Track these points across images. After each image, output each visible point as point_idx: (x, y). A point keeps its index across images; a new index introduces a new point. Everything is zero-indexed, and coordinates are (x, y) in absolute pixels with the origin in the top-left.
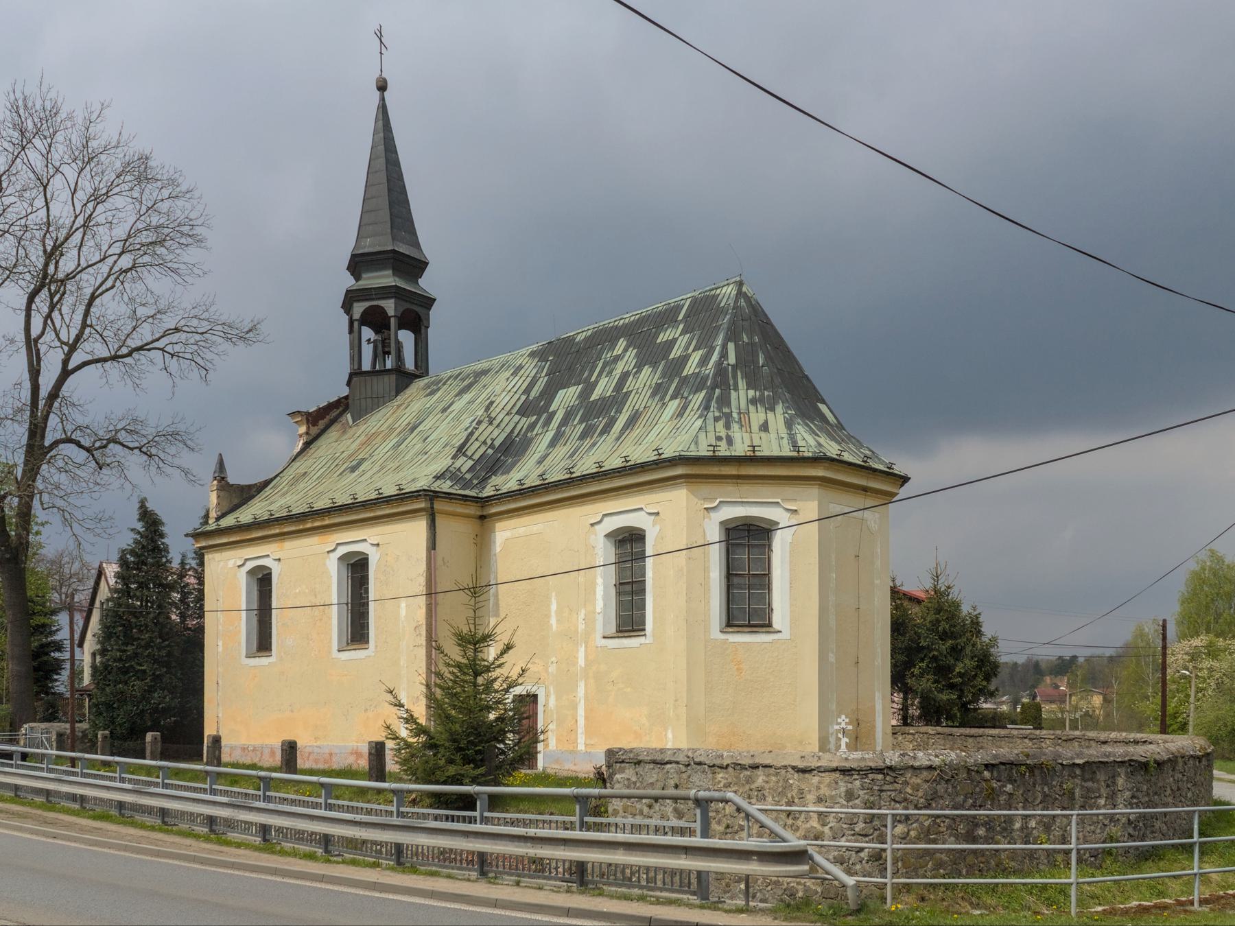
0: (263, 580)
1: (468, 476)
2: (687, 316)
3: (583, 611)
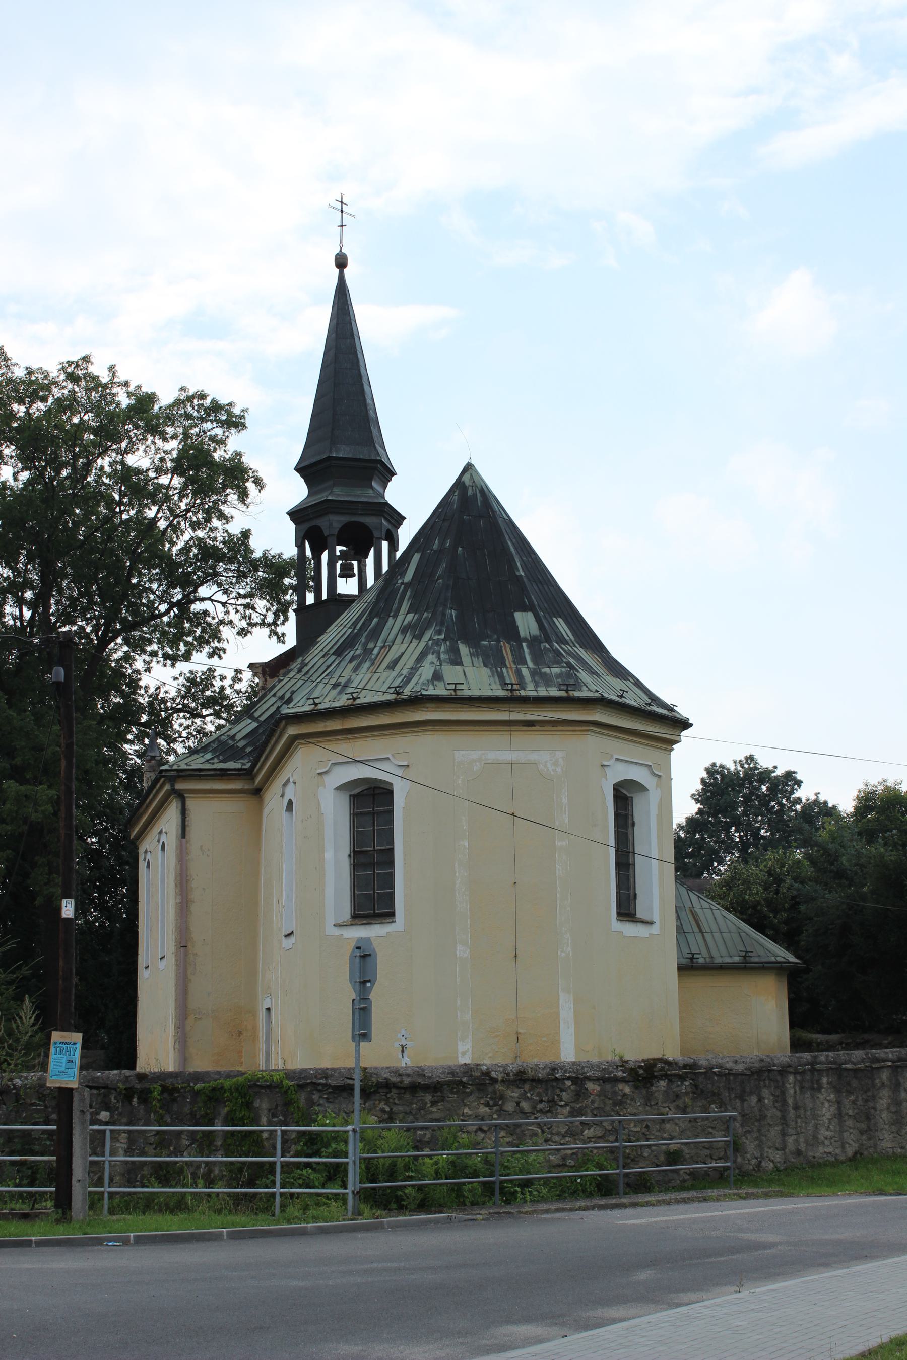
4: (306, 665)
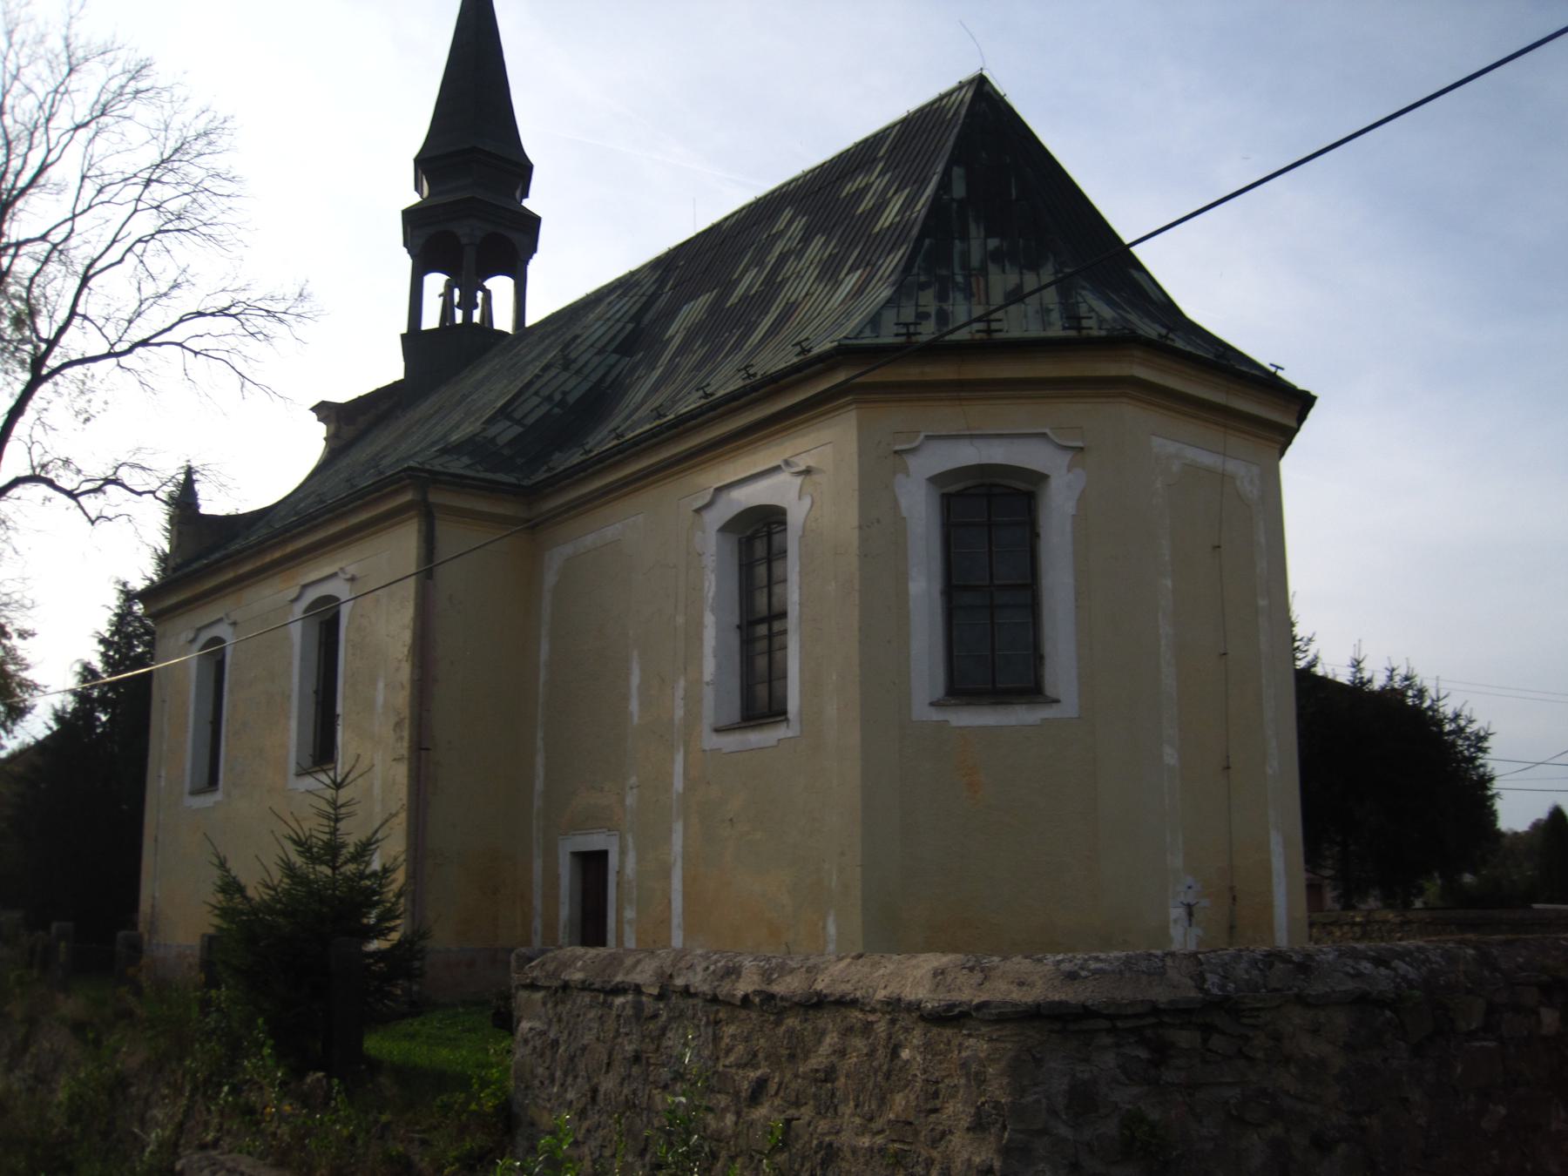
1: (506, 452)
2: (891, 151)
3: (682, 683)
4: (575, 361)
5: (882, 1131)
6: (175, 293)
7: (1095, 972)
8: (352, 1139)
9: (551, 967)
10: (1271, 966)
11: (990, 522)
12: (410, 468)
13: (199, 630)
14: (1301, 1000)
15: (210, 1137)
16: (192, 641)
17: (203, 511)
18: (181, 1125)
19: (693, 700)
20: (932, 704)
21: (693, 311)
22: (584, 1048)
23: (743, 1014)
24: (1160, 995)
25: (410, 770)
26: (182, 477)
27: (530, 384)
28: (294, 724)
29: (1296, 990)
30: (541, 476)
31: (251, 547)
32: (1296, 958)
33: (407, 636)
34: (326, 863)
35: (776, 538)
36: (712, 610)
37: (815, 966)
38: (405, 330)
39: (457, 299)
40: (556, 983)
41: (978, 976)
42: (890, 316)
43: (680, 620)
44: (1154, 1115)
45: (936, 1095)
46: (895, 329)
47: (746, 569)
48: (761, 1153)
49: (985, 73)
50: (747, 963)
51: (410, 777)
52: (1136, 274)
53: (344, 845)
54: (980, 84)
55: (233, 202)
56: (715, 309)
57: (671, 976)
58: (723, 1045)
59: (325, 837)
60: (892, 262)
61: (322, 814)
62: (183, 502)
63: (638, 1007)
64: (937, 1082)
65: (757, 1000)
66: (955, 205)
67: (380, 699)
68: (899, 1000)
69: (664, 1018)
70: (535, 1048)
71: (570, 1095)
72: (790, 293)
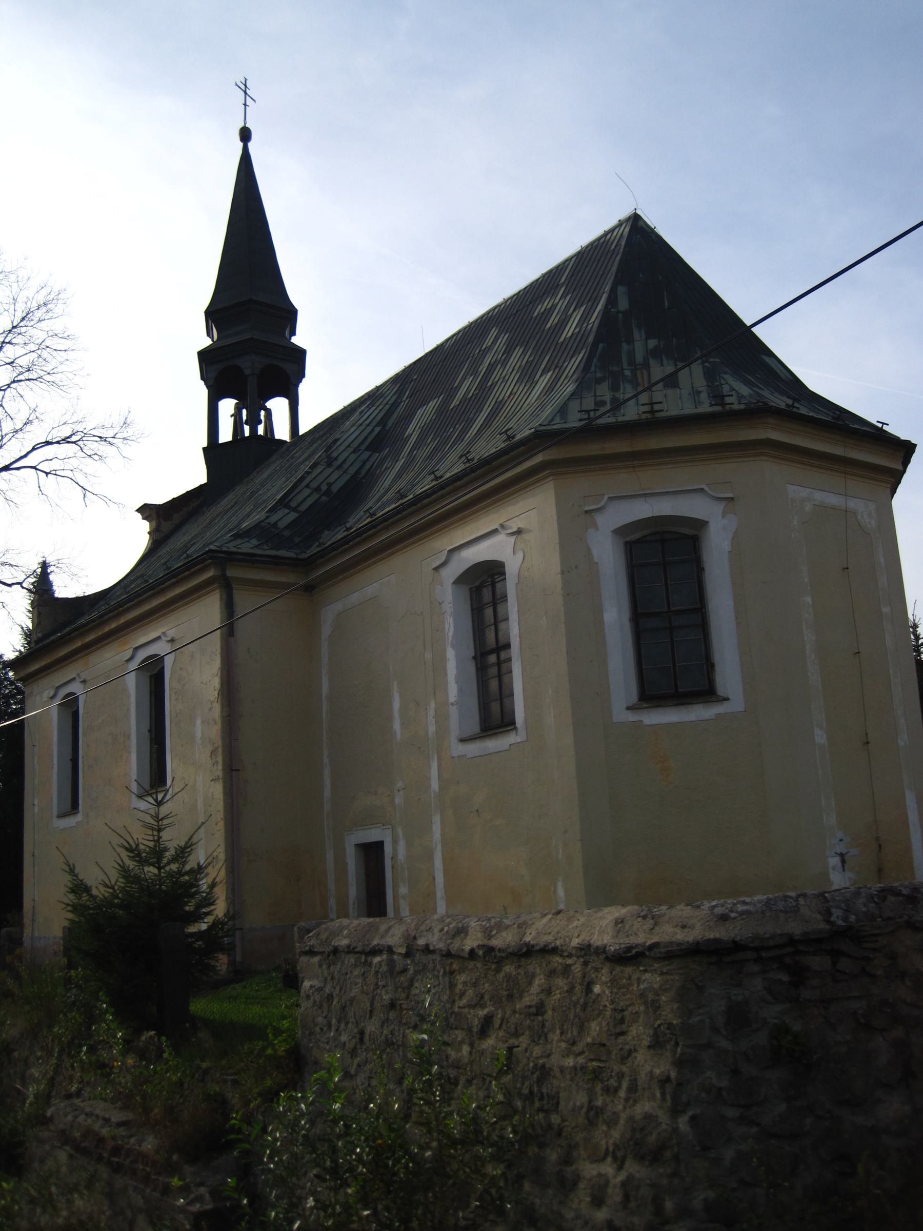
0: (71, 706)
1: (286, 533)
5: (582, 1053)
6: (29, 427)
7: (742, 913)
8: (181, 1084)
9: (323, 937)
10: (884, 899)
11: (664, 562)
12: (210, 551)
13: (58, 688)
14: (911, 925)
15: (74, 1088)
16: (52, 698)
17: (56, 595)
18: (52, 1080)
19: (441, 718)
20: (628, 708)
21: (426, 413)
22: (352, 1000)
23: (471, 964)
24: (795, 928)
25: (225, 787)
26: (39, 570)
27: (302, 479)
28: (134, 757)
29: (906, 918)
30: (314, 550)
31: (93, 621)
32: (905, 892)
33: (216, 682)
34: (153, 865)
35: (498, 586)
36: (453, 646)
37: (525, 923)
38: (205, 445)
39: (244, 418)
40: (327, 949)
41: (650, 923)
42: (574, 405)
43: (428, 656)
44: (797, 1027)
45: (622, 1021)
46: (579, 416)
47: (477, 611)
48: (489, 1075)
49: (638, 212)
50: (473, 924)
51: (225, 793)
52: (767, 359)
53: (166, 849)
54: (635, 220)
55: (70, 355)
56: (441, 411)
57: (415, 938)
58: (457, 991)
59: (151, 844)
60: (574, 364)
61: (147, 826)
62: (42, 587)
63: (391, 963)
64: (623, 1011)
65: (481, 953)
66: (620, 315)
67: (199, 734)
68: (589, 946)
69: (411, 972)
70: (315, 1002)
71: (344, 1038)
72: (501, 392)
